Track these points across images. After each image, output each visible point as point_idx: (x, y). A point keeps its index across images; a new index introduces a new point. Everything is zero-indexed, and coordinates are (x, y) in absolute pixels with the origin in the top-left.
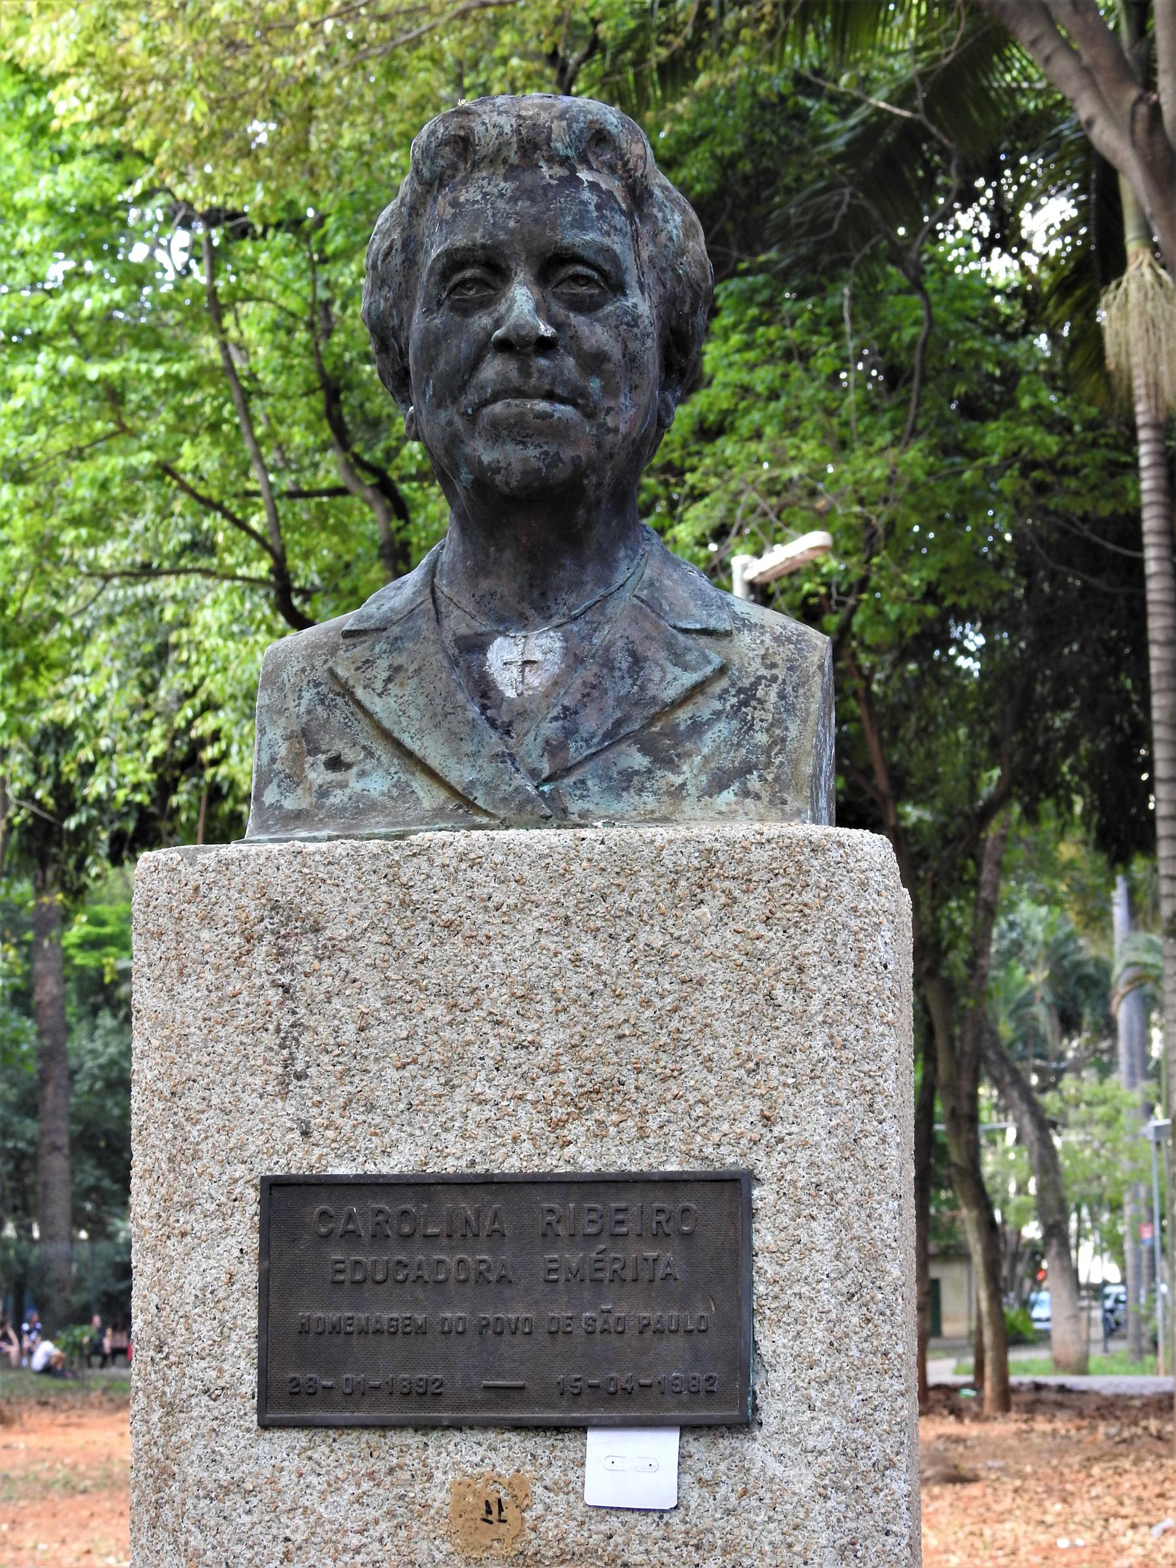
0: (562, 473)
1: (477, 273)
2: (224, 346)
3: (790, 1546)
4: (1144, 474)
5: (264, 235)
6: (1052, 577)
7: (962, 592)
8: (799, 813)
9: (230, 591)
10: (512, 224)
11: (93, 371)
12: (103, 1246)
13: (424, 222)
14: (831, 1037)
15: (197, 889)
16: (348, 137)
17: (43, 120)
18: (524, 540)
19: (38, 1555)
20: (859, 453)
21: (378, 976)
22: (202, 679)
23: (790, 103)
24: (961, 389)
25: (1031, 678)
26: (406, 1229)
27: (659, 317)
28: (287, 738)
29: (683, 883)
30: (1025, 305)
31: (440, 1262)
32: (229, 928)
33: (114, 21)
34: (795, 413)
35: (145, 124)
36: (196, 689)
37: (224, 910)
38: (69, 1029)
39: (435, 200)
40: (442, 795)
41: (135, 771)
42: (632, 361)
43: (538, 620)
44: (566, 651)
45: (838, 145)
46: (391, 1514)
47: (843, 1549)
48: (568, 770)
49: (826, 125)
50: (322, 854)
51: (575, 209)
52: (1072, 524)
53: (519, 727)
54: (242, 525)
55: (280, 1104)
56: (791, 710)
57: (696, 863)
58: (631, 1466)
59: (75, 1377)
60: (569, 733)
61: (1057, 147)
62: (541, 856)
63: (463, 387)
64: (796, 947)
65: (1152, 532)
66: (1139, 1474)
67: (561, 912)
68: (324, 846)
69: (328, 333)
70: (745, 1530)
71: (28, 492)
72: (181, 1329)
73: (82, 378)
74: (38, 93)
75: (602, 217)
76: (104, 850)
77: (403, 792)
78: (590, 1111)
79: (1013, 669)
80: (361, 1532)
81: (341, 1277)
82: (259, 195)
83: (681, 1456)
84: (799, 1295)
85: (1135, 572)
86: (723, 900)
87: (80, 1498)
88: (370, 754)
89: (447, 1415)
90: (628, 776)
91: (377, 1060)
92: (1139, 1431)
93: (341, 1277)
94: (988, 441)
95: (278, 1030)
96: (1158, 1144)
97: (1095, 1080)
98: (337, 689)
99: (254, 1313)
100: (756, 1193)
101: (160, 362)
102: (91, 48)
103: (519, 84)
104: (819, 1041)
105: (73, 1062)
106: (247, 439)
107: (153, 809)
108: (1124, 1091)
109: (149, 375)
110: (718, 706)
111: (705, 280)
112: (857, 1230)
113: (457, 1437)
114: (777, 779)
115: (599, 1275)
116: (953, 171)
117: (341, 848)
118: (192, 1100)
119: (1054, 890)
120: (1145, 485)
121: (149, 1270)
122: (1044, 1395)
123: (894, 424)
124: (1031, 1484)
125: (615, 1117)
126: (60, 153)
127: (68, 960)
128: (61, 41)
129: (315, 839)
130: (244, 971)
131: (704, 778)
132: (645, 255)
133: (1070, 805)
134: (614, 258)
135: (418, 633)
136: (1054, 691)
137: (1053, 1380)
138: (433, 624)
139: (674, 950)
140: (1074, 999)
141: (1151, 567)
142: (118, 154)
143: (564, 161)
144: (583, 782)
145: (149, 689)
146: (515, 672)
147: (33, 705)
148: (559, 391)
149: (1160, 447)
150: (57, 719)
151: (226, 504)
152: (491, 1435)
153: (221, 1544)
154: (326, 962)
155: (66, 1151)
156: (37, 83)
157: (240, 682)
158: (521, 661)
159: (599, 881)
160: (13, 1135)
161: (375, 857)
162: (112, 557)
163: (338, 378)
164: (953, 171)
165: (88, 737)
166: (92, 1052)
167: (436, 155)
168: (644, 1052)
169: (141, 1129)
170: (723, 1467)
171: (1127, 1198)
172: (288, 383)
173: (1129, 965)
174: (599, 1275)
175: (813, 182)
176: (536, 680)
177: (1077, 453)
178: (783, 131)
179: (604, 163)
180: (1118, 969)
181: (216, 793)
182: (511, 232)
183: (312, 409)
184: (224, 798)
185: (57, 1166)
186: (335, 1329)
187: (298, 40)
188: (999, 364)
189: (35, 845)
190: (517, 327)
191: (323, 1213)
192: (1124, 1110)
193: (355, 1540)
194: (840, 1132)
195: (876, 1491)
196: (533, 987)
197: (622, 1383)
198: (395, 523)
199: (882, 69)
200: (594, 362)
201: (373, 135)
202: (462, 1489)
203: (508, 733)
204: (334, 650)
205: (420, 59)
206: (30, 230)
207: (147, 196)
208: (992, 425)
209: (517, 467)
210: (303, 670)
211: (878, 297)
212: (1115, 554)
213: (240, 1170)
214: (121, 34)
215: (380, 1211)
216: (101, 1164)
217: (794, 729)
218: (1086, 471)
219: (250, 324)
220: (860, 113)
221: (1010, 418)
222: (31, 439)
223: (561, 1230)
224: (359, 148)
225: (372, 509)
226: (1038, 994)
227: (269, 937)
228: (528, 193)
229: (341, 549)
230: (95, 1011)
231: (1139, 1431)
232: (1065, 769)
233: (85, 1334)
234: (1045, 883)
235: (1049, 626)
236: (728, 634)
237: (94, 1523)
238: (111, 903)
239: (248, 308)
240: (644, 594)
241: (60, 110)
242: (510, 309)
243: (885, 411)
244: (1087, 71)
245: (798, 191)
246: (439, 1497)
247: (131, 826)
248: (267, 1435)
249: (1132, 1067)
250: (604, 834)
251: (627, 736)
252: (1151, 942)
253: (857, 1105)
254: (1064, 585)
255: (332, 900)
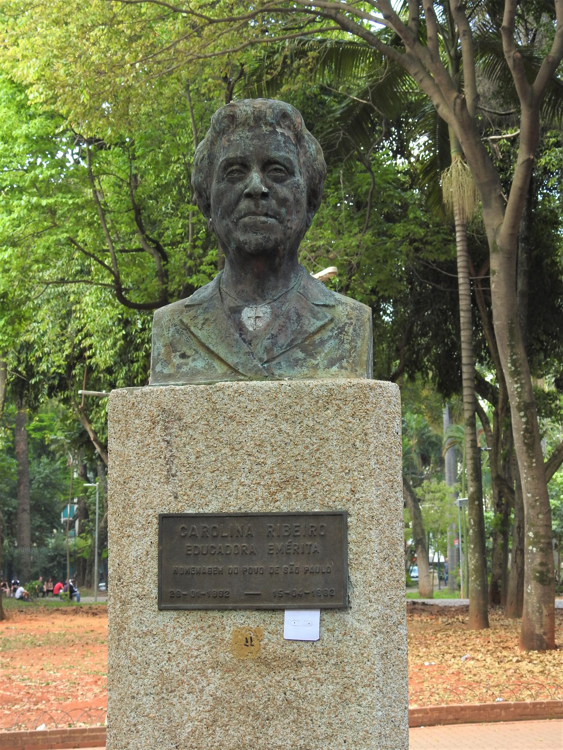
0: (270, 245)
1: (238, 167)
2: (95, 192)
3: (362, 654)
4: (458, 244)
5: (110, 148)
6: (421, 285)
7: (386, 290)
8: (362, 375)
9: (96, 289)
10: (251, 149)
11: (44, 202)
12: (43, 549)
13: (216, 147)
14: (377, 460)
15: (133, 404)
16: (144, 109)
17: (23, 102)
18: (256, 270)
19: (22, 670)
20: (346, 236)
21: (203, 437)
22: (85, 324)
23: (319, 97)
24: (386, 210)
25: (412, 325)
26: (215, 534)
27: (307, 185)
28: (164, 346)
29: (321, 401)
30: (411, 177)
31: (228, 546)
32: (146, 419)
33: (52, 63)
34: (321, 220)
35: (64, 103)
36: (82, 328)
37: (144, 412)
38: (30, 463)
39: (221, 139)
40: (225, 368)
41: (59, 360)
42: (297, 201)
43: (261, 301)
44: (272, 313)
45: (338, 114)
46: (209, 643)
47: (382, 655)
48: (274, 358)
49: (333, 106)
50: (182, 390)
51: (276, 143)
52: (429, 263)
53: (254, 342)
54: (102, 263)
55: (166, 486)
56: (358, 335)
57: (326, 394)
58: (301, 624)
59: (32, 601)
60: (274, 344)
61: (423, 116)
62: (266, 391)
63: (232, 212)
64: (364, 426)
65: (461, 267)
66: (455, 636)
67: (274, 412)
68: (183, 387)
69: (136, 187)
70: (345, 648)
71: (18, 250)
72: (128, 572)
73: (40, 205)
74: (21, 91)
75: (286, 146)
76: (46, 392)
77: (210, 367)
78: (285, 489)
79: (405, 321)
80: (198, 650)
81: (190, 552)
82: (109, 132)
83: (321, 620)
84: (366, 559)
85: (454, 283)
86: (336, 408)
87: (38, 648)
88: (197, 352)
89: (231, 605)
90: (297, 361)
91: (203, 469)
92: (455, 620)
93: (190, 552)
94: (397, 231)
95: (165, 458)
96: (461, 508)
97: (436, 483)
98: (183, 327)
99: (156, 566)
100: (349, 520)
101: (70, 198)
102: (43, 73)
103: (212, 89)
104: (373, 462)
105: (31, 477)
106: (104, 229)
107: (65, 376)
108: (447, 487)
109: (66, 203)
110: (330, 334)
111: (324, 171)
112: (387, 534)
113: (235, 613)
114: (353, 362)
115: (289, 551)
116: (383, 125)
117: (189, 388)
118: (132, 485)
119: (420, 408)
120: (458, 249)
121: (115, 550)
122: (416, 606)
123: (359, 224)
124: (413, 641)
125: (295, 491)
126: (30, 115)
127: (29, 435)
128: (32, 70)
129: (177, 385)
130: (152, 435)
131: (325, 361)
132: (301, 161)
133: (427, 374)
134: (291, 162)
135: (215, 306)
136: (421, 330)
137: (420, 601)
138: (220, 302)
139: (317, 427)
140: (427, 451)
141: (461, 281)
142: (52, 115)
143: (271, 125)
144: (280, 363)
145: (64, 328)
146: (252, 321)
147: (17, 335)
148: (270, 213)
149: (464, 234)
150: (27, 340)
151: (96, 255)
152: (248, 613)
153: (144, 655)
154: (184, 432)
155: (28, 511)
156: (21, 88)
157: (100, 326)
158: (255, 317)
159: (288, 401)
160: (8, 505)
161: (202, 391)
162: (49, 276)
163: (140, 205)
164: (383, 125)
165: (39, 347)
166: (39, 472)
167: (222, 122)
168: (306, 466)
169: (111, 496)
170: (336, 624)
171: (448, 529)
172: (120, 206)
173: (450, 437)
174: (289, 551)
175: (327, 129)
176: (260, 324)
177: (431, 236)
178: (315, 109)
179: (286, 126)
180: (445, 439)
181: (90, 369)
182: (251, 152)
183: (130, 218)
184: (94, 371)
185: (25, 517)
186: (188, 573)
187: (125, 71)
188: (400, 201)
189: (18, 390)
190: (254, 188)
191: (183, 528)
192: (447, 494)
193: (195, 653)
194: (381, 496)
195: (395, 633)
196: (263, 441)
197: (298, 593)
198: (163, 263)
199: (354, 85)
200: (283, 202)
201: (153, 109)
202: (237, 633)
203: (250, 344)
204: (182, 312)
205: (172, 79)
206: (19, 146)
207: (64, 132)
208: (398, 225)
209: (254, 242)
210: (170, 320)
211: (353, 174)
212: (446, 276)
213: (151, 512)
214: (55, 68)
215: (205, 527)
216: (42, 516)
217: (359, 343)
218: (435, 243)
219: (105, 183)
220: (346, 102)
221: (405, 222)
222: (19, 229)
223: (274, 534)
224: (148, 114)
225: (153, 257)
226: (413, 449)
227: (161, 422)
228: (258, 137)
229: (141, 273)
230: (40, 456)
231: (455, 620)
232: (425, 360)
233: (36, 584)
234: (416, 405)
235: (419, 305)
236: (333, 306)
237: (44, 658)
238: (47, 413)
239: (104, 177)
240: (301, 291)
241: (31, 97)
242: (251, 181)
243: (356, 219)
244: (437, 86)
245: (322, 132)
246: (228, 636)
247: (56, 382)
248: (162, 613)
249: (450, 477)
250: (288, 383)
251: (296, 346)
252: (458, 428)
253: (387, 486)
254: (425, 288)
255: (186, 408)
